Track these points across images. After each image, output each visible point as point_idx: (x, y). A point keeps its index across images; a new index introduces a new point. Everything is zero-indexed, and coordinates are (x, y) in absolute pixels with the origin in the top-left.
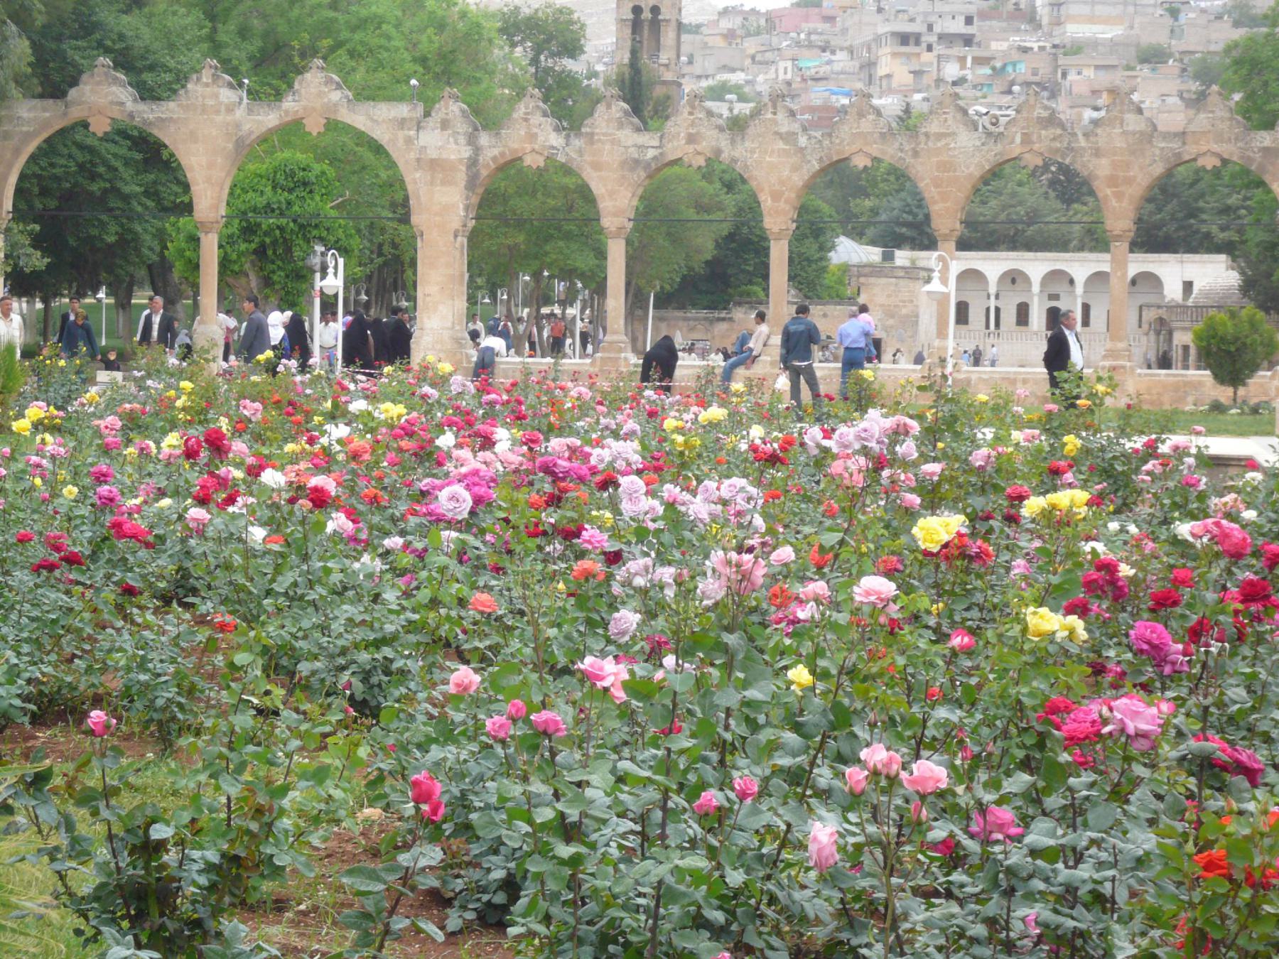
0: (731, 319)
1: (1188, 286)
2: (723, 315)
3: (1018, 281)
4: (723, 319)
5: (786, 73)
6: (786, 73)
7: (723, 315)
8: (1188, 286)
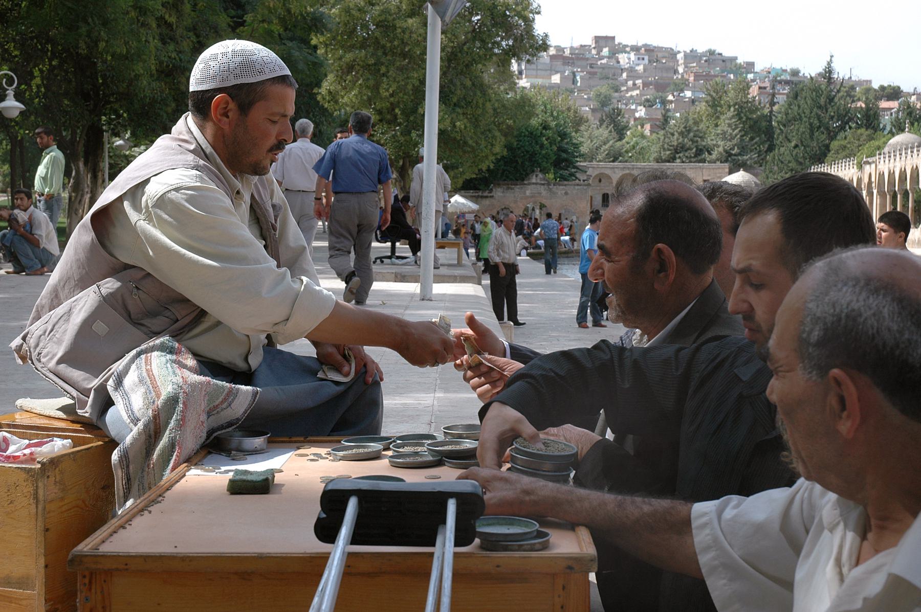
0: (492, 197)
2: (486, 194)
3: (603, 180)
4: (487, 197)
7: (486, 194)
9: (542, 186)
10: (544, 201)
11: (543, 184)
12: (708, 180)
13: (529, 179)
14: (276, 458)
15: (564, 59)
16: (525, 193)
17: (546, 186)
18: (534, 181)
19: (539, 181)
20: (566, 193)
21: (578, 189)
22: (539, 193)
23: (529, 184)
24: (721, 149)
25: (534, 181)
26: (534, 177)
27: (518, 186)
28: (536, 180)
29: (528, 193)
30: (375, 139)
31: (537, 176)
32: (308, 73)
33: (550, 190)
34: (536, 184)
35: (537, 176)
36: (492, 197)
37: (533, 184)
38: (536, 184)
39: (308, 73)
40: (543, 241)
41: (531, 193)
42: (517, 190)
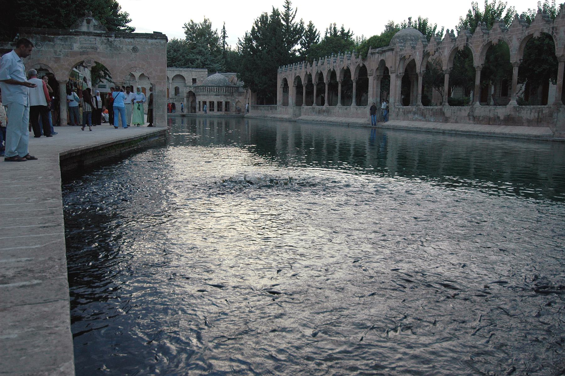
1: (194, 80)
5: (159, 289)
6: (159, 289)
9: (98, 38)
11: (99, 35)
13: (77, 26)
16: (71, 47)
18: (84, 29)
19: (92, 30)
20: (135, 50)
21: (152, 44)
22: (93, 48)
23: (78, 34)
24: (199, 61)
25: (84, 29)
26: (85, 23)
28: (88, 27)
29: (76, 47)
31: (88, 22)
33: (110, 44)
34: (88, 34)
35: (88, 22)
37: (84, 33)
38: (88, 34)
41: (82, 48)
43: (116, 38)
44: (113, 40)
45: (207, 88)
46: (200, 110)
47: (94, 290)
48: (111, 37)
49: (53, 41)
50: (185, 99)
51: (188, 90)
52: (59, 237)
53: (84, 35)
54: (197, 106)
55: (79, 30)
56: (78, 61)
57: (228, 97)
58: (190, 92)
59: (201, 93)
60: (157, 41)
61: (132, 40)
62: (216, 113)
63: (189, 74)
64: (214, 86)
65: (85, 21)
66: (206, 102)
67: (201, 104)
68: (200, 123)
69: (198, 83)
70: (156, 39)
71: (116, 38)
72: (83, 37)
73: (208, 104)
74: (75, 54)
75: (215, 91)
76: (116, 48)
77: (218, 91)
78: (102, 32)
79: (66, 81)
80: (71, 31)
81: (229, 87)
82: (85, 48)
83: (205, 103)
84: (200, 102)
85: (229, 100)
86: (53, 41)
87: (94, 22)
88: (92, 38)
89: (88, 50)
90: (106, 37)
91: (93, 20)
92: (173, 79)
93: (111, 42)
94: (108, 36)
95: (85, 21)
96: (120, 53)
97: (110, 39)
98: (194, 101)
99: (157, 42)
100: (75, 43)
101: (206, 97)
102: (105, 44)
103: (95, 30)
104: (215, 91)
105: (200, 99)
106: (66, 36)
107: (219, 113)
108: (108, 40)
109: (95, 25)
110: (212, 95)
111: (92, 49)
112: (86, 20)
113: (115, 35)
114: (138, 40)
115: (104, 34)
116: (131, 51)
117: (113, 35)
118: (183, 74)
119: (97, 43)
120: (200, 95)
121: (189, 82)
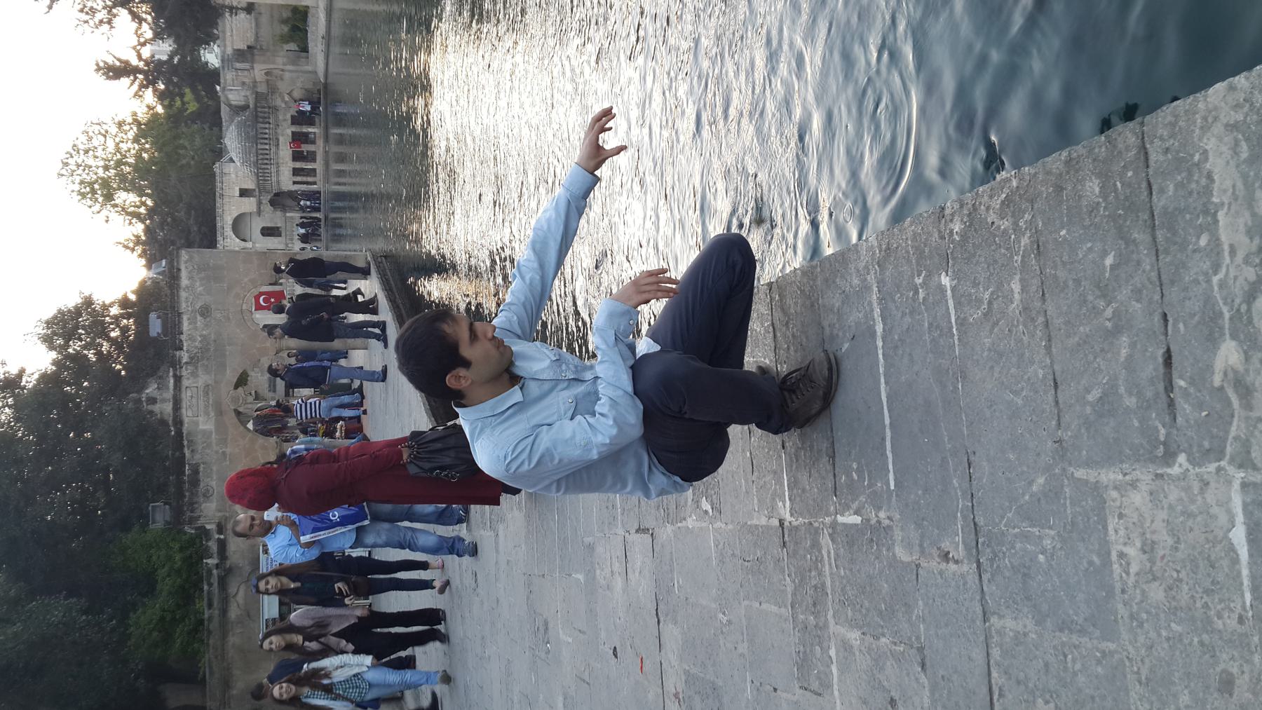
1: (244, 193)
8: (244, 193)
9: (185, 383)
10: (231, 376)
11: (178, 379)
12: (1213, 181)
13: (163, 422)
14: (411, 385)
15: (421, 673)
16: (206, 434)
17: (184, 373)
19: (169, 394)
20: (205, 312)
21: (191, 278)
23: (178, 422)
25: (168, 408)
26: (156, 408)
27: (187, 452)
28: (164, 401)
30: (493, 310)
32: (914, 618)
35: (153, 401)
36: (221, 529)
39: (914, 618)
40: (248, 426)
41: (207, 414)
42: (197, 457)
43: (182, 349)
44: (186, 354)
45: (261, 164)
46: (315, 183)
47: (341, 540)
48: (180, 358)
49: (197, 465)
50: (288, 215)
51: (267, 208)
52: (483, 514)
53: (180, 408)
54: (304, 187)
55: (171, 418)
56: (236, 420)
57: (281, 118)
58: (272, 203)
59: (274, 179)
60: (183, 267)
61: (185, 317)
62: (319, 148)
63: (230, 207)
64: (257, 149)
65: (150, 407)
66: (294, 169)
67: (299, 179)
68: (340, 184)
69: (250, 185)
70: (179, 270)
71: (182, 349)
72: (184, 411)
73: (298, 165)
74: (220, 426)
75: (267, 147)
76: (204, 349)
77: (266, 141)
78: (171, 374)
79: (277, 442)
80: (173, 433)
81: (257, 116)
82: (206, 407)
83: (296, 172)
84: (295, 183)
85: (289, 117)
86: (197, 465)
87: (151, 390)
88: (186, 396)
89: (211, 402)
90: (181, 368)
91: (147, 391)
92: (244, 240)
93: (192, 358)
94: (175, 364)
95: (150, 407)
96: (215, 341)
97: (184, 360)
98: (292, 195)
99: (186, 268)
100: (197, 424)
101: (281, 168)
102: (196, 368)
103: (168, 388)
104: (267, 147)
105: (286, 182)
106: (185, 443)
107: (319, 157)
108: (186, 363)
109: (159, 388)
110: (277, 153)
111: (208, 394)
112: (147, 405)
113: (176, 350)
114: (184, 305)
115: (174, 371)
116: (208, 319)
117: (178, 353)
118: (229, 220)
119: (195, 385)
120: (278, 182)
121: (249, 205)
